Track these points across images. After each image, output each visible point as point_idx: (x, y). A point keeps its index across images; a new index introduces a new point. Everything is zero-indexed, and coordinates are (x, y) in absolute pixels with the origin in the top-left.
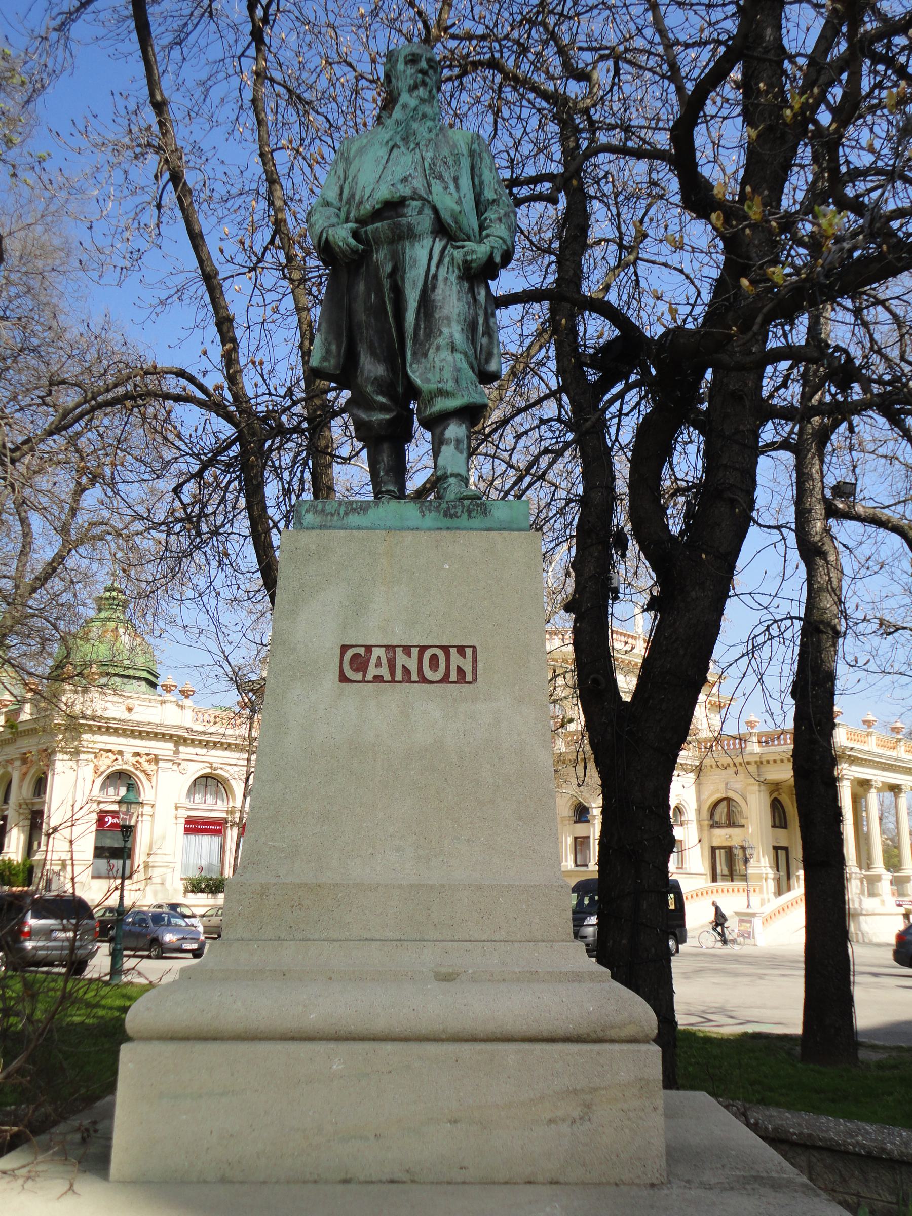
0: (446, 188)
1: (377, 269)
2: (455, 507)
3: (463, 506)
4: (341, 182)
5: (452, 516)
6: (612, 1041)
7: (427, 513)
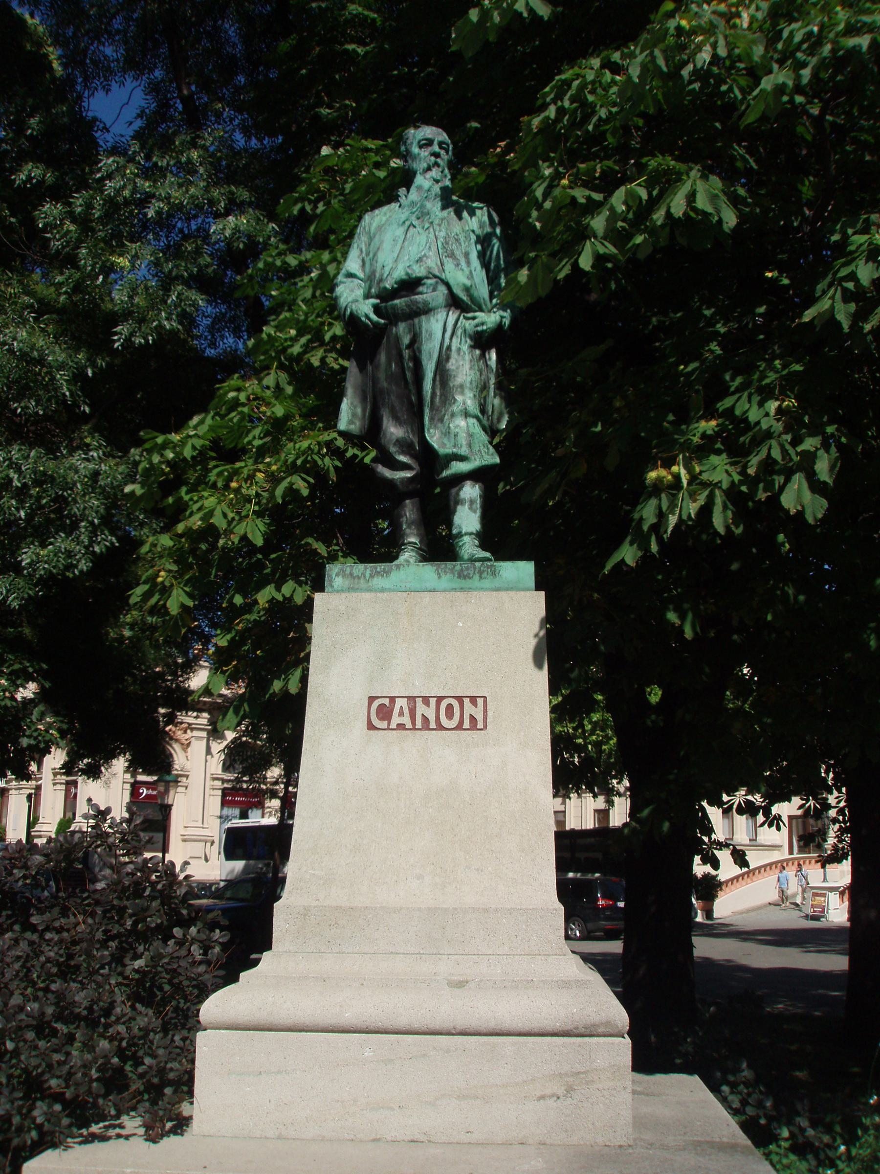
0: (458, 265)
1: (397, 339)
2: (467, 569)
5: (465, 578)
6: (599, 1036)
7: (442, 574)
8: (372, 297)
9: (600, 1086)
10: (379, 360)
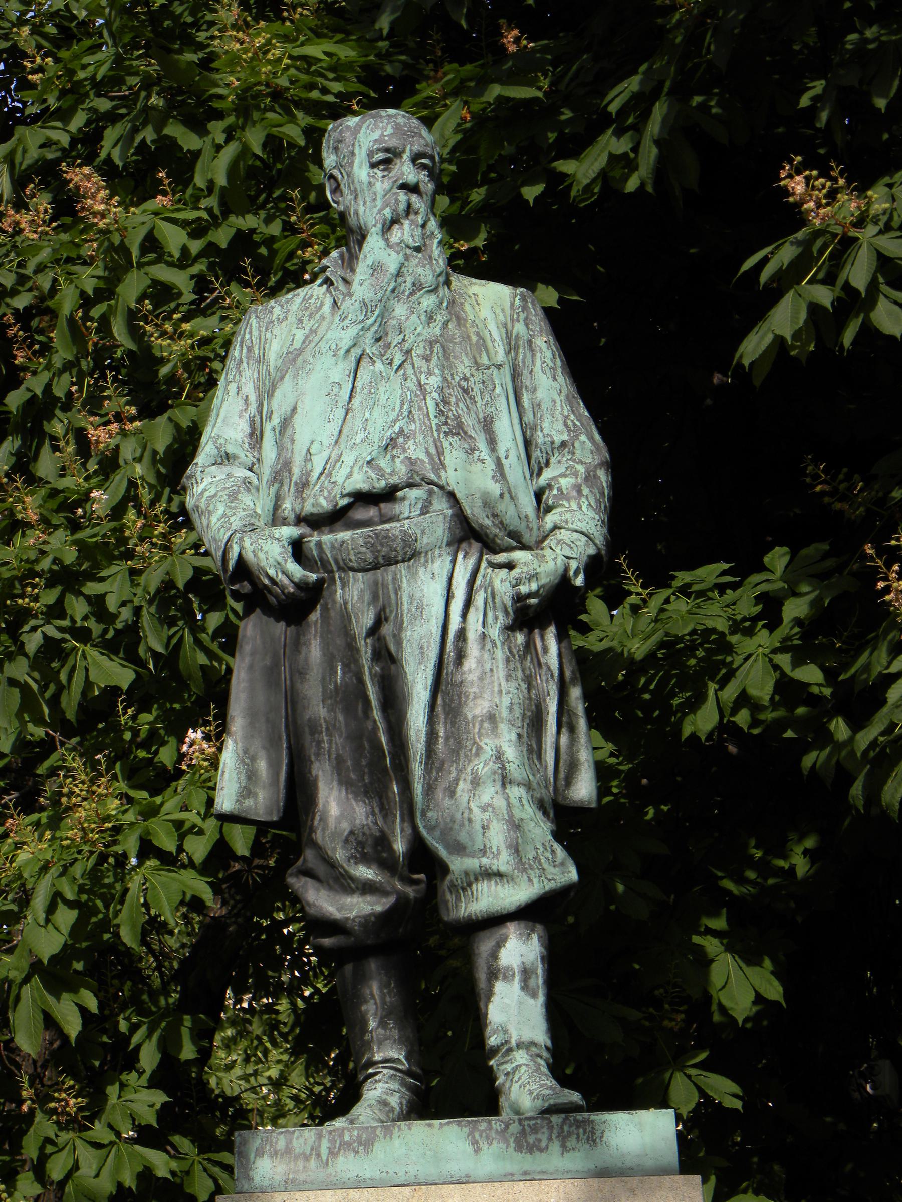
1: (346, 618)
3: (551, 1128)
4: (253, 409)
8: (284, 522)
10: (306, 660)
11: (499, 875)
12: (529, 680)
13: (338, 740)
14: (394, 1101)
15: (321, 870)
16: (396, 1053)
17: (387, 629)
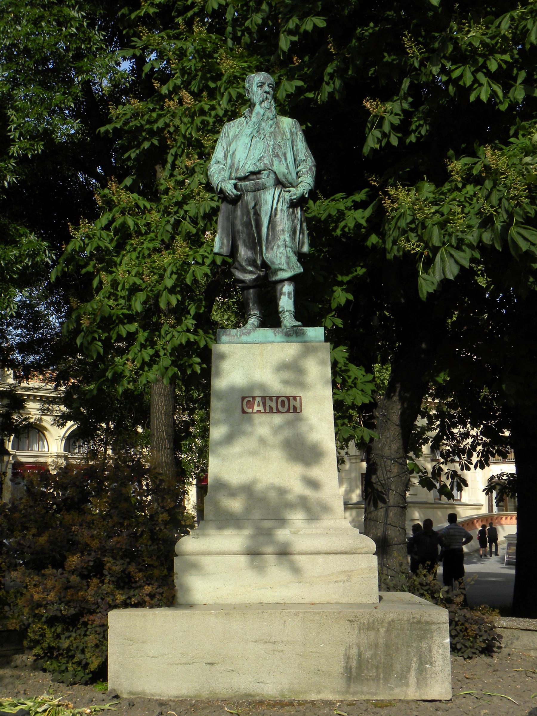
1: (247, 204)
4: (225, 150)
8: (232, 179)
9: (363, 576)
11: (283, 270)
12: (293, 221)
13: (244, 235)
14: (256, 323)
15: (239, 267)
16: (257, 312)
17: (257, 207)
